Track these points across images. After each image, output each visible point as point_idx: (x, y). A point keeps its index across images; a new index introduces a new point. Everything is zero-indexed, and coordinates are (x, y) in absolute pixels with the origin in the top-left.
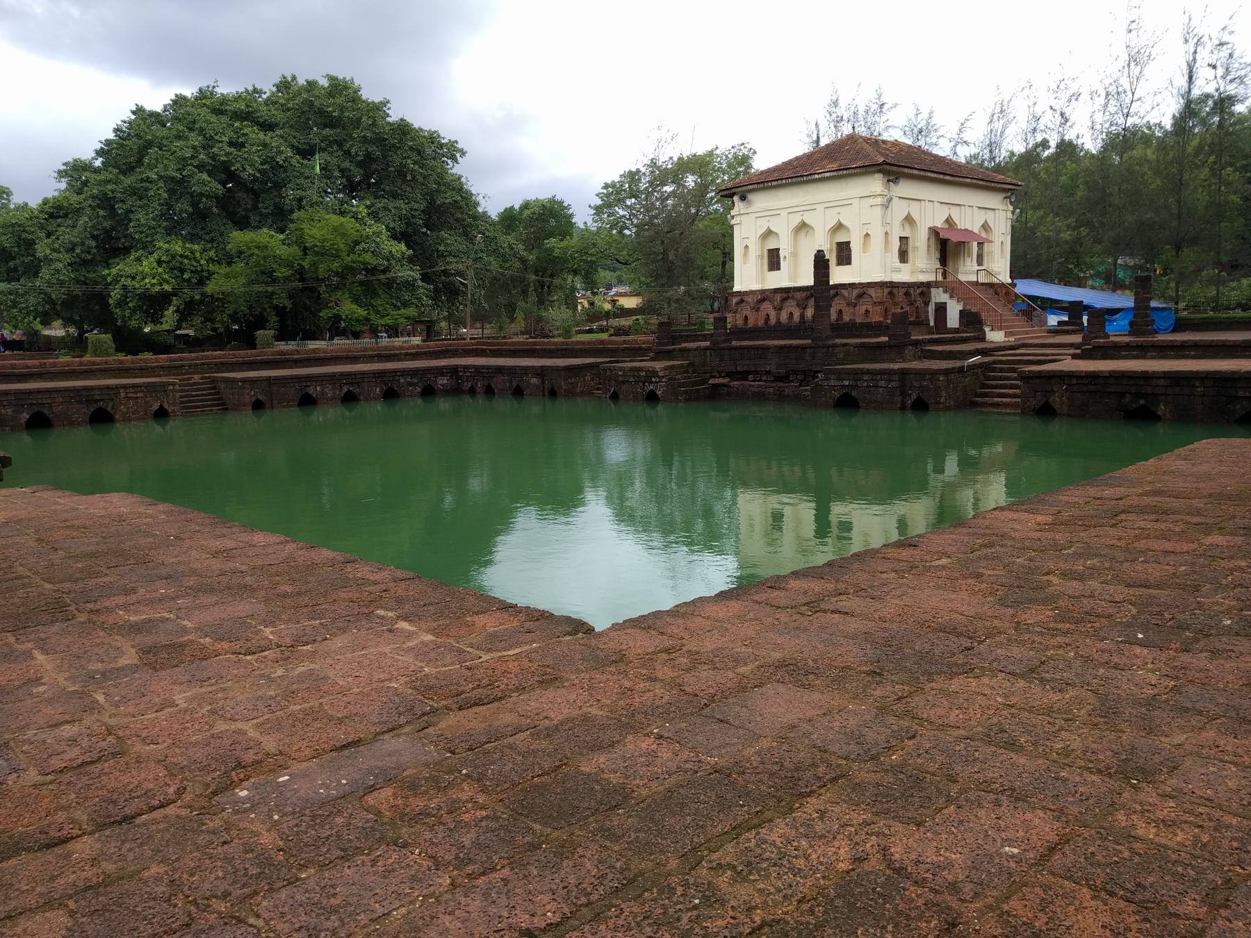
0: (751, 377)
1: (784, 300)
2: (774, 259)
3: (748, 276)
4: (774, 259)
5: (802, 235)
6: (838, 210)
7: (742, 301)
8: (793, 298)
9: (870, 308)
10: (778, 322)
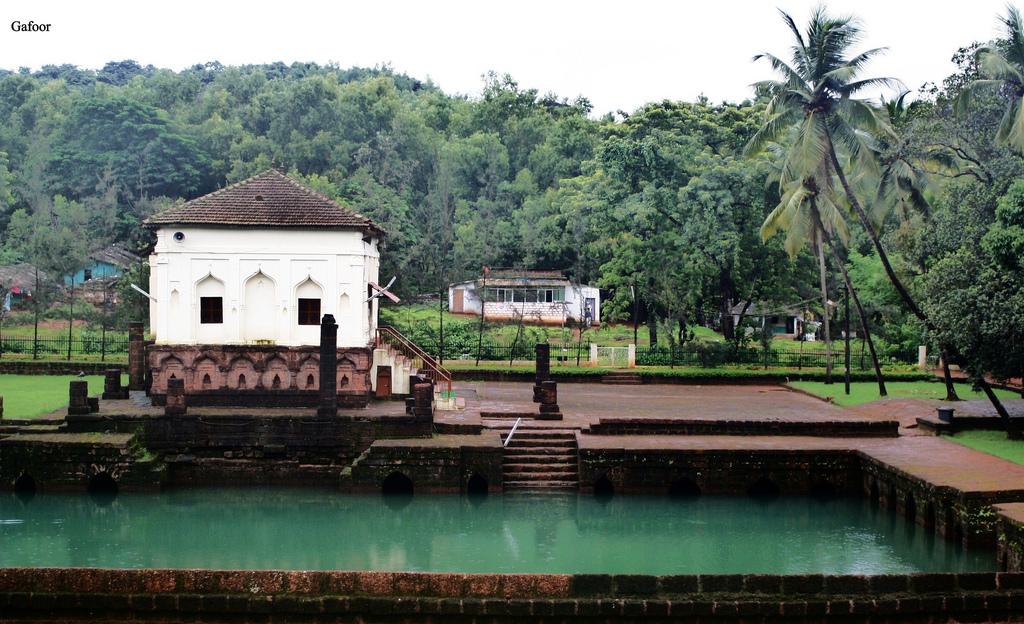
0: (229, 453)
1: (234, 360)
2: (212, 310)
3: (173, 322)
4: (212, 310)
5: (256, 282)
6: (259, 262)
7: (171, 357)
8: (249, 360)
9: (349, 375)
10: (294, 387)
